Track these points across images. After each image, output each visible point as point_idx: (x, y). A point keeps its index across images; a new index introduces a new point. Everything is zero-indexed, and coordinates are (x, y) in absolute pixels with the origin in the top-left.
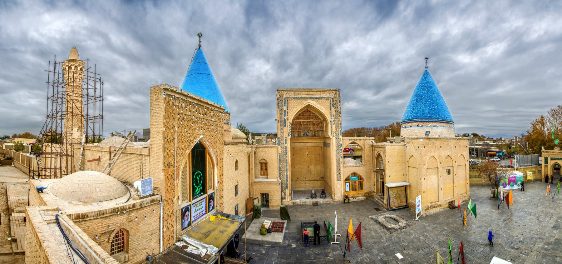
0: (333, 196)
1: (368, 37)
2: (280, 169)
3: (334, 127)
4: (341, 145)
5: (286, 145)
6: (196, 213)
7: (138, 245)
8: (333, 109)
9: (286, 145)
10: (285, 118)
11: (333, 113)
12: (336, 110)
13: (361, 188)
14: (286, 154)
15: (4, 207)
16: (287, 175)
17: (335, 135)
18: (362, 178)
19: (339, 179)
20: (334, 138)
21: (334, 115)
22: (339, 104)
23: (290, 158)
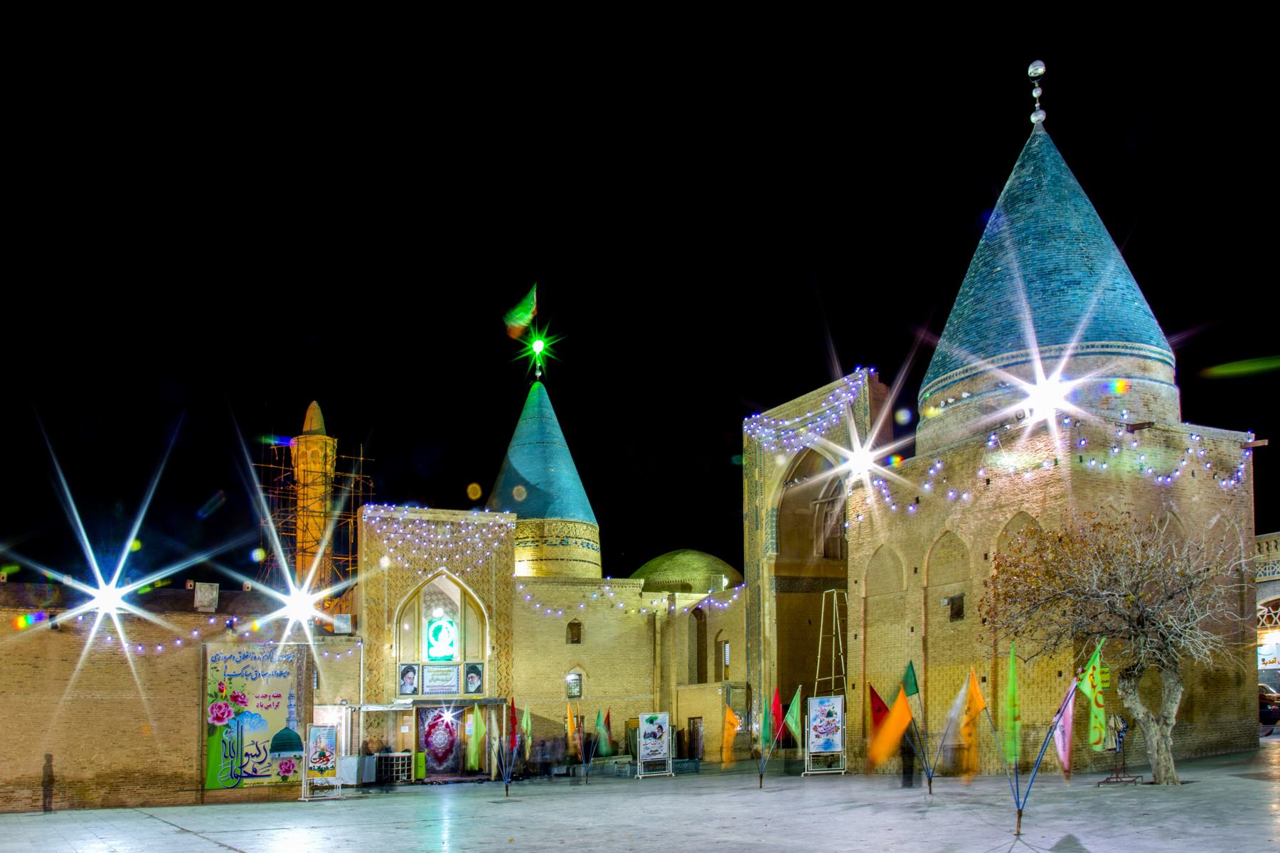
6: (433, 683)
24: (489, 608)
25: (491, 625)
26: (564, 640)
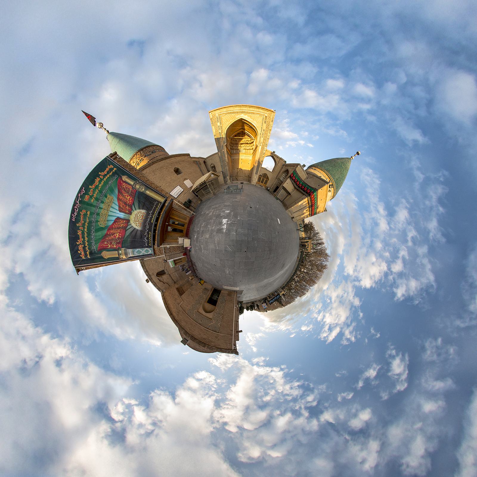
0: (251, 181)
1: (236, 385)
2: (221, 165)
3: (262, 139)
4: (264, 153)
5: (223, 150)
7: (161, 267)
8: (265, 125)
9: (223, 150)
10: (220, 131)
11: (264, 128)
12: (267, 127)
13: (266, 183)
14: (224, 156)
15: (208, 417)
16: (227, 169)
17: (261, 144)
18: (268, 179)
19: (256, 173)
20: (261, 147)
21: (264, 130)
22: (271, 123)
23: (227, 158)
26: (176, 175)
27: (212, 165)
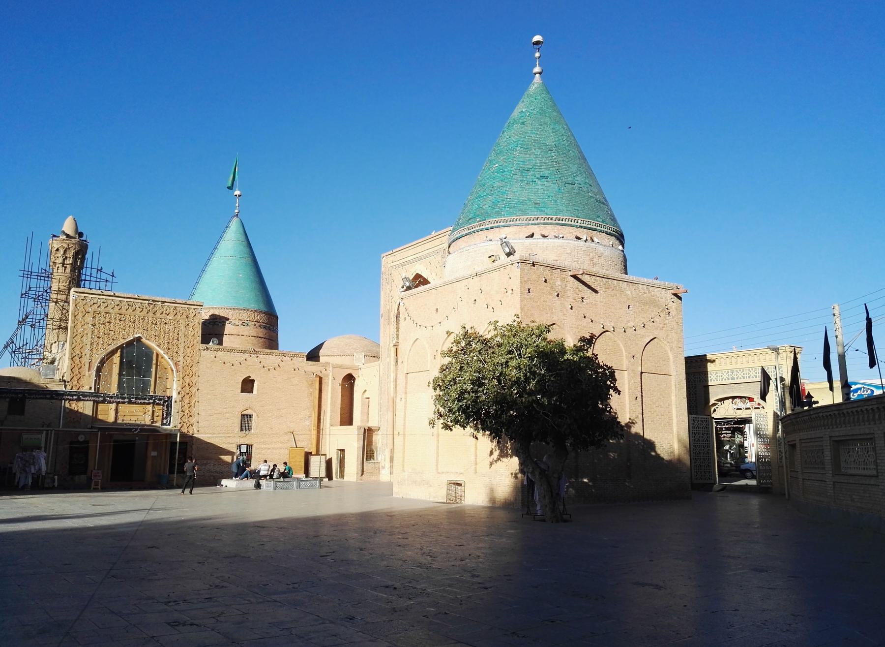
2: (380, 404)
5: (388, 360)
24: (176, 364)
25: (178, 376)
27: (366, 395)
